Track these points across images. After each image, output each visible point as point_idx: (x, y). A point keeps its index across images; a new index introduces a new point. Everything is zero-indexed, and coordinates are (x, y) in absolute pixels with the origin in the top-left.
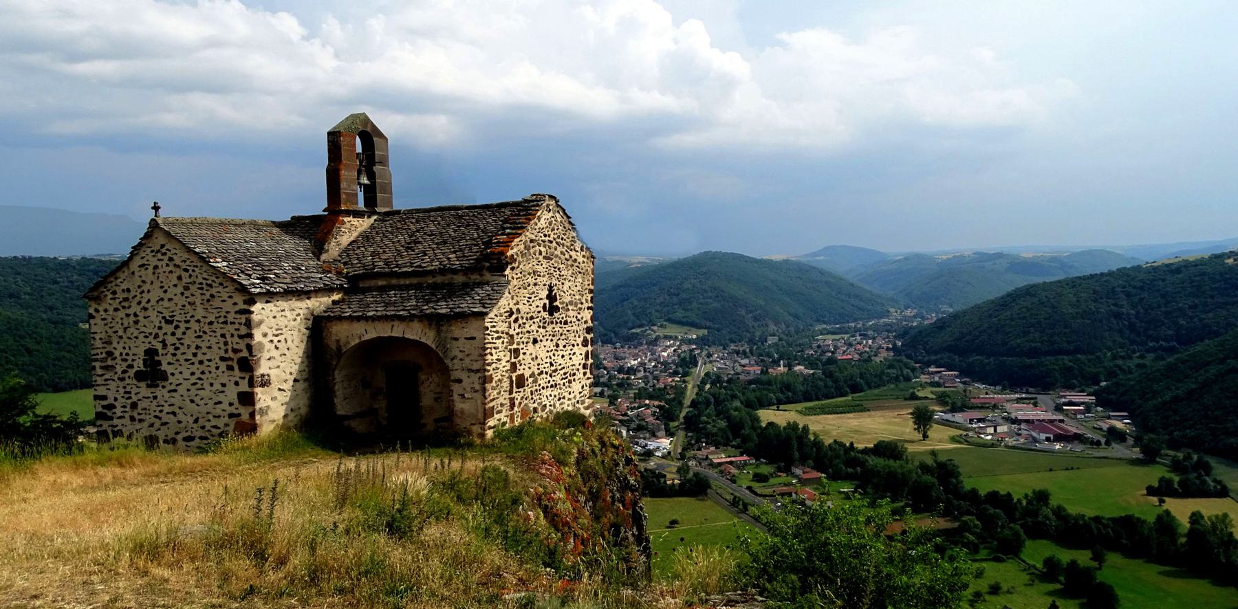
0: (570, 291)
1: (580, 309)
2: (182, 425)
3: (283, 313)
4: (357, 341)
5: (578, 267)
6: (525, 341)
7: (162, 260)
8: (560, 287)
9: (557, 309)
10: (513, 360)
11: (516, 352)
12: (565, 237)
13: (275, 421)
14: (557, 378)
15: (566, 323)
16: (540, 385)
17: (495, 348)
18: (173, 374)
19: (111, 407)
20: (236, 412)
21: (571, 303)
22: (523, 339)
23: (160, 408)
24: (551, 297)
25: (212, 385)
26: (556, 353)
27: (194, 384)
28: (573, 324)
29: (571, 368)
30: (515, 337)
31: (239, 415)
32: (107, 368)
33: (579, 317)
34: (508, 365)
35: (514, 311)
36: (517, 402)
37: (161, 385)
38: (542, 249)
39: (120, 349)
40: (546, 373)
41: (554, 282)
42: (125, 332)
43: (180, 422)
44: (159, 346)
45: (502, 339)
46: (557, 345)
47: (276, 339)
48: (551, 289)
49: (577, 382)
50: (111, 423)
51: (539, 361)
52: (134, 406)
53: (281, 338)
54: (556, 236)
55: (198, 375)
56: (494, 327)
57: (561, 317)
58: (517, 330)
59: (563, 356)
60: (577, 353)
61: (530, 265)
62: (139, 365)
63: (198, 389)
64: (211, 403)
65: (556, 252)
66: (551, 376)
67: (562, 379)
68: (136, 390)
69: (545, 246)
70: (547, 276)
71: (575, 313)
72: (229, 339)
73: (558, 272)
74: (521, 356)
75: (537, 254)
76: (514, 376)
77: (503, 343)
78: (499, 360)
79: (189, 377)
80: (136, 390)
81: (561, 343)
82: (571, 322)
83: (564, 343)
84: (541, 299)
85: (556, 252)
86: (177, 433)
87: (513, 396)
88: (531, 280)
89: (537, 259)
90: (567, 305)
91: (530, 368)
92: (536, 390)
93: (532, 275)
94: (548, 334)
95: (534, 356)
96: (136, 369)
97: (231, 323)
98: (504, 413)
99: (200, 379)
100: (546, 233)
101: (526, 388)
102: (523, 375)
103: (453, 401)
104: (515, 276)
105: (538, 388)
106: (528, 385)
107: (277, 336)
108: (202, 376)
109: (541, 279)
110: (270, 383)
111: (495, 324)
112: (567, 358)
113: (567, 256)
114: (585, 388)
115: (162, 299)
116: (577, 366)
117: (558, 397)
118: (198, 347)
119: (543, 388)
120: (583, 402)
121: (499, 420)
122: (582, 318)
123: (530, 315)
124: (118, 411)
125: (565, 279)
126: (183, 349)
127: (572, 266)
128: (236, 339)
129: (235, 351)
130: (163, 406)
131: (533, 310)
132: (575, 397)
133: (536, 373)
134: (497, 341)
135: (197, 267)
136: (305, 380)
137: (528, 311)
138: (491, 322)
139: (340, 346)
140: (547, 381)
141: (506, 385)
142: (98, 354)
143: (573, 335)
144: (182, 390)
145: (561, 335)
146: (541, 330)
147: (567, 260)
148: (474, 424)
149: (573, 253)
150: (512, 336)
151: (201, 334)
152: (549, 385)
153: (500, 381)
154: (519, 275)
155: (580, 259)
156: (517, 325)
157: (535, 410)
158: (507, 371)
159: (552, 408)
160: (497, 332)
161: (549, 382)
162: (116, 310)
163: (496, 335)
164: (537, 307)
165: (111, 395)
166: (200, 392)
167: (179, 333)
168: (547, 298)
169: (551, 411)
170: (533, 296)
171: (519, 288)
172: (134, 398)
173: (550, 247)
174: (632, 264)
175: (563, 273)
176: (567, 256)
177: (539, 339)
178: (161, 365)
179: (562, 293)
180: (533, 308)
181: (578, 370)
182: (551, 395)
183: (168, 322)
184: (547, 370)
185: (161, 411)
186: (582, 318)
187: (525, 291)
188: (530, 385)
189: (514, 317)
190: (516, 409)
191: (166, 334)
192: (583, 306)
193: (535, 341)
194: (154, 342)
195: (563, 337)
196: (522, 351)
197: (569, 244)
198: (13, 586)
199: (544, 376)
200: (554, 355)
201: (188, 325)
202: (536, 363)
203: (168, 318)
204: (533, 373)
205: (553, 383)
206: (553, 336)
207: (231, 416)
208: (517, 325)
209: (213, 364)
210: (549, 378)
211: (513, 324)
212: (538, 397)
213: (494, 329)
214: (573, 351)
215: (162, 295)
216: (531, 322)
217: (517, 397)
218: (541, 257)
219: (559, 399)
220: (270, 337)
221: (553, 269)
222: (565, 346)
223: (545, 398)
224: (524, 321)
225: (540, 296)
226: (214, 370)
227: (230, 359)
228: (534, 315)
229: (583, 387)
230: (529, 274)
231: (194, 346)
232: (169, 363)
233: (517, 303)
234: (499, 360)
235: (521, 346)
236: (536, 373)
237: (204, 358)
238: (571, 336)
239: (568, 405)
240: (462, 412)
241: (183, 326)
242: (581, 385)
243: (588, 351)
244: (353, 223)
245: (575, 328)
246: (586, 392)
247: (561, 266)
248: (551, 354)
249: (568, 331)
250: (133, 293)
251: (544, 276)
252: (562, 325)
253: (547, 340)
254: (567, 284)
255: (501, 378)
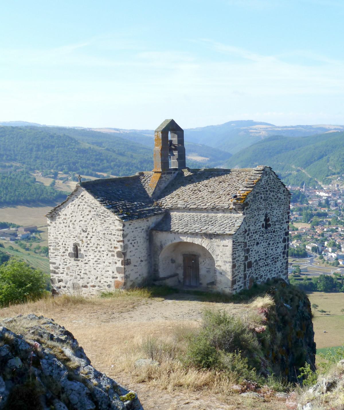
0: (277, 215)
1: (282, 223)
2: (90, 280)
3: (136, 229)
4: (170, 243)
5: (281, 201)
6: (252, 244)
7: (82, 202)
8: (272, 214)
9: (270, 225)
10: (246, 255)
11: (248, 251)
12: (275, 187)
13: (132, 281)
14: (269, 261)
15: (274, 232)
16: (259, 266)
17: (237, 251)
18: (86, 256)
19: (58, 268)
20: (115, 276)
21: (277, 221)
22: (252, 244)
23: (80, 271)
24: (267, 220)
25: (104, 262)
26: (269, 248)
27: (96, 261)
28: (278, 232)
29: (276, 255)
30: (248, 243)
31: (117, 278)
32: (56, 249)
33: (281, 228)
34: (244, 258)
35: (247, 230)
36: (247, 276)
37: (80, 260)
38: (263, 196)
39: (62, 241)
40: (263, 259)
41: (268, 211)
42: (64, 234)
43: (89, 278)
44: (80, 243)
45: (241, 246)
46: (269, 244)
47: (133, 242)
48: (266, 216)
49: (279, 261)
50: (57, 275)
51: (259, 253)
52: (68, 268)
53: (135, 241)
54: (270, 188)
55: (98, 257)
56: (237, 240)
57: (271, 229)
58: (249, 239)
59: (272, 249)
60: (280, 247)
61: (256, 205)
62: (71, 250)
63: (98, 264)
64: (104, 271)
65: (270, 196)
66: (265, 260)
67: (271, 261)
68: (69, 261)
69: (264, 194)
70: (265, 209)
71: (279, 226)
72: (113, 242)
73: (271, 206)
74: (250, 252)
75: (260, 199)
76: (246, 262)
77: (241, 247)
78: (239, 256)
79: (94, 258)
80: (69, 261)
81: (271, 243)
82: (277, 231)
83: (273, 242)
84: (261, 222)
85: (270, 196)
86: (88, 283)
87: (246, 272)
88: (256, 213)
89: (259, 201)
90: (275, 222)
91: (254, 258)
92: (258, 268)
93: (257, 210)
94: (264, 239)
95: (257, 251)
96: (69, 252)
97: (114, 235)
98: (241, 282)
99: (99, 259)
100: (265, 187)
101: (252, 268)
102: (251, 261)
103: (216, 276)
104: (248, 213)
105: (258, 267)
106: (253, 266)
107: (134, 240)
108: (100, 258)
109: (261, 212)
110: (130, 263)
111: (238, 239)
112: (274, 250)
113: (276, 197)
114: (283, 264)
115: (82, 221)
116: (280, 253)
117: (269, 270)
118: (98, 244)
119: (261, 267)
120: (282, 272)
121: (239, 285)
122: (283, 228)
123: (255, 231)
124: (61, 270)
125: (274, 209)
126: (91, 245)
127: (278, 201)
128: (115, 242)
129: (115, 248)
130: (81, 270)
131: (257, 228)
132: (278, 269)
133: (258, 260)
134: (239, 247)
135: (98, 207)
136: (146, 260)
137: (255, 229)
138: (235, 238)
139: (162, 245)
140: (263, 263)
141: (242, 267)
142: (51, 243)
143: (278, 237)
144: (91, 263)
145: (271, 238)
146: (261, 238)
147: (276, 199)
148: (227, 288)
149: (279, 195)
150: (246, 243)
151: (100, 238)
152: (264, 265)
153: (239, 266)
154: (250, 212)
155: (283, 197)
156: (248, 237)
157: (257, 278)
158: (243, 261)
159: (265, 277)
160: (239, 242)
161: (264, 263)
162: (60, 223)
163: (238, 244)
164: (259, 226)
165: (58, 263)
166: (98, 265)
167: (89, 237)
168: (264, 221)
169: (265, 278)
170: (257, 221)
171: (250, 218)
172: (68, 265)
173: (266, 194)
174: (331, 130)
175: (273, 206)
176: (276, 197)
177: (259, 242)
178: (81, 251)
179: (272, 217)
180: (257, 227)
181: (280, 255)
182: (265, 270)
183: (83, 231)
184: (263, 257)
185: (81, 272)
186: (283, 228)
187: (253, 219)
188: (254, 266)
189: (247, 233)
190: (247, 279)
191: (83, 237)
192: (283, 222)
193: (258, 244)
194: (77, 240)
195: (273, 239)
196: (250, 250)
197: (276, 191)
198: (274, 388)
199: (262, 261)
200: (267, 249)
201: (93, 234)
202: (258, 255)
203: (84, 229)
204: (256, 260)
205: (266, 264)
206: (267, 239)
207: (113, 278)
208: (248, 237)
209: (105, 253)
210: (264, 262)
211: (246, 237)
212: (258, 272)
213: (237, 241)
214: (278, 246)
215: (82, 219)
216: (256, 234)
217: (248, 273)
218: (262, 200)
219: (270, 271)
220: (131, 241)
221: (268, 205)
222: (273, 244)
223: (262, 272)
224: (252, 234)
225: (261, 220)
226: (105, 256)
227: (113, 251)
228: (257, 230)
229: (282, 264)
230: (255, 210)
231: (96, 244)
232: (85, 251)
233: (249, 226)
234: (239, 256)
235: (251, 247)
236: (258, 260)
237: (101, 250)
238: (277, 238)
239: (274, 274)
240: (221, 281)
241: (91, 234)
242: (281, 263)
243: (286, 245)
244: (166, 177)
245: (279, 234)
246: (284, 267)
247: (272, 203)
248: (266, 249)
249: (275, 236)
250: (68, 216)
251: (263, 209)
252: (272, 233)
253: (264, 242)
254: (275, 211)
255: (240, 265)
